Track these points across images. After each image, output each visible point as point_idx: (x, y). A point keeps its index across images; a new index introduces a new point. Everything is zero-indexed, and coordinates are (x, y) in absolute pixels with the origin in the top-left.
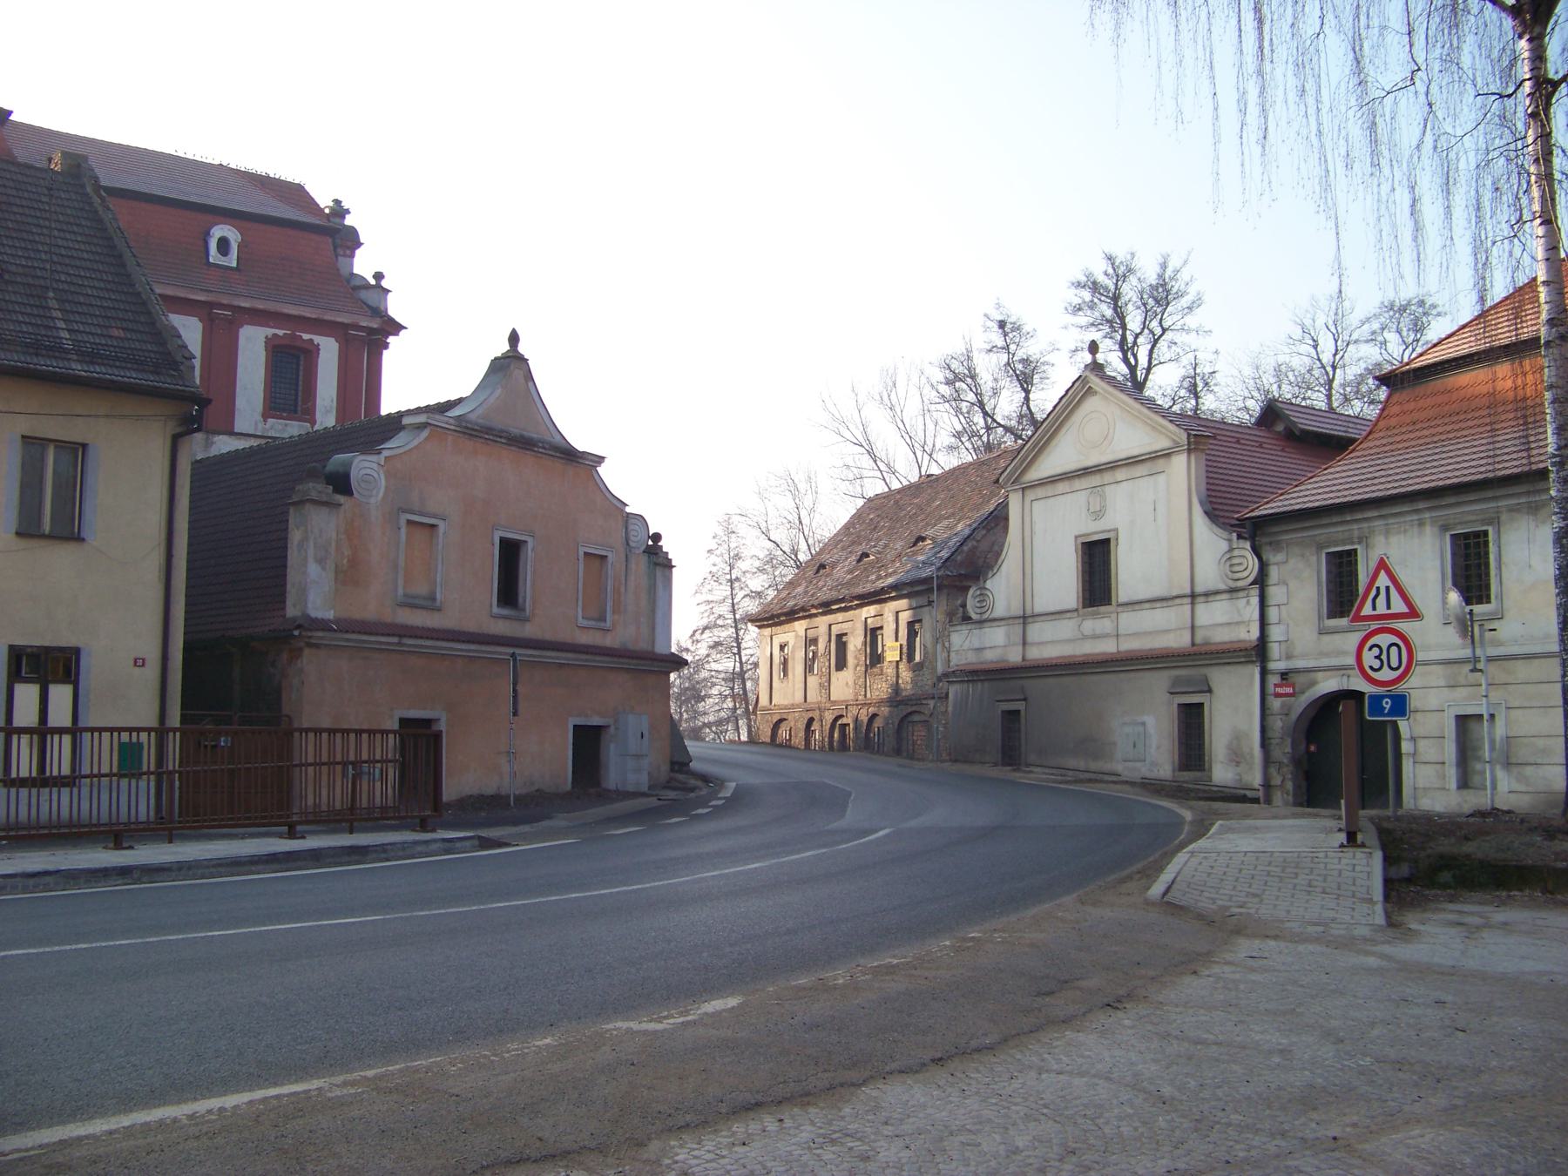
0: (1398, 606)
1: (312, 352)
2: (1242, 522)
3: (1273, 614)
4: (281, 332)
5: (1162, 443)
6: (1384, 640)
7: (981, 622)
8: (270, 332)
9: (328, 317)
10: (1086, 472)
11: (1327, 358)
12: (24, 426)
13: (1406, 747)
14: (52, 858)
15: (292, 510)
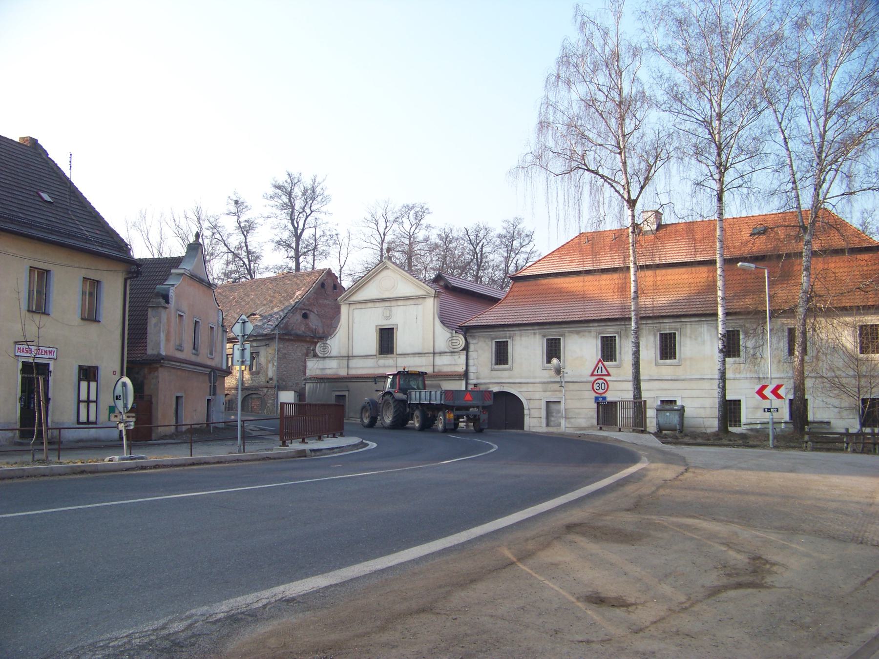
0: (604, 372)
2: (461, 327)
3: (471, 362)
5: (421, 293)
6: (600, 381)
7: (324, 358)
10: (383, 300)
11: (382, 231)
12: (84, 273)
13: (526, 412)
15: (149, 309)
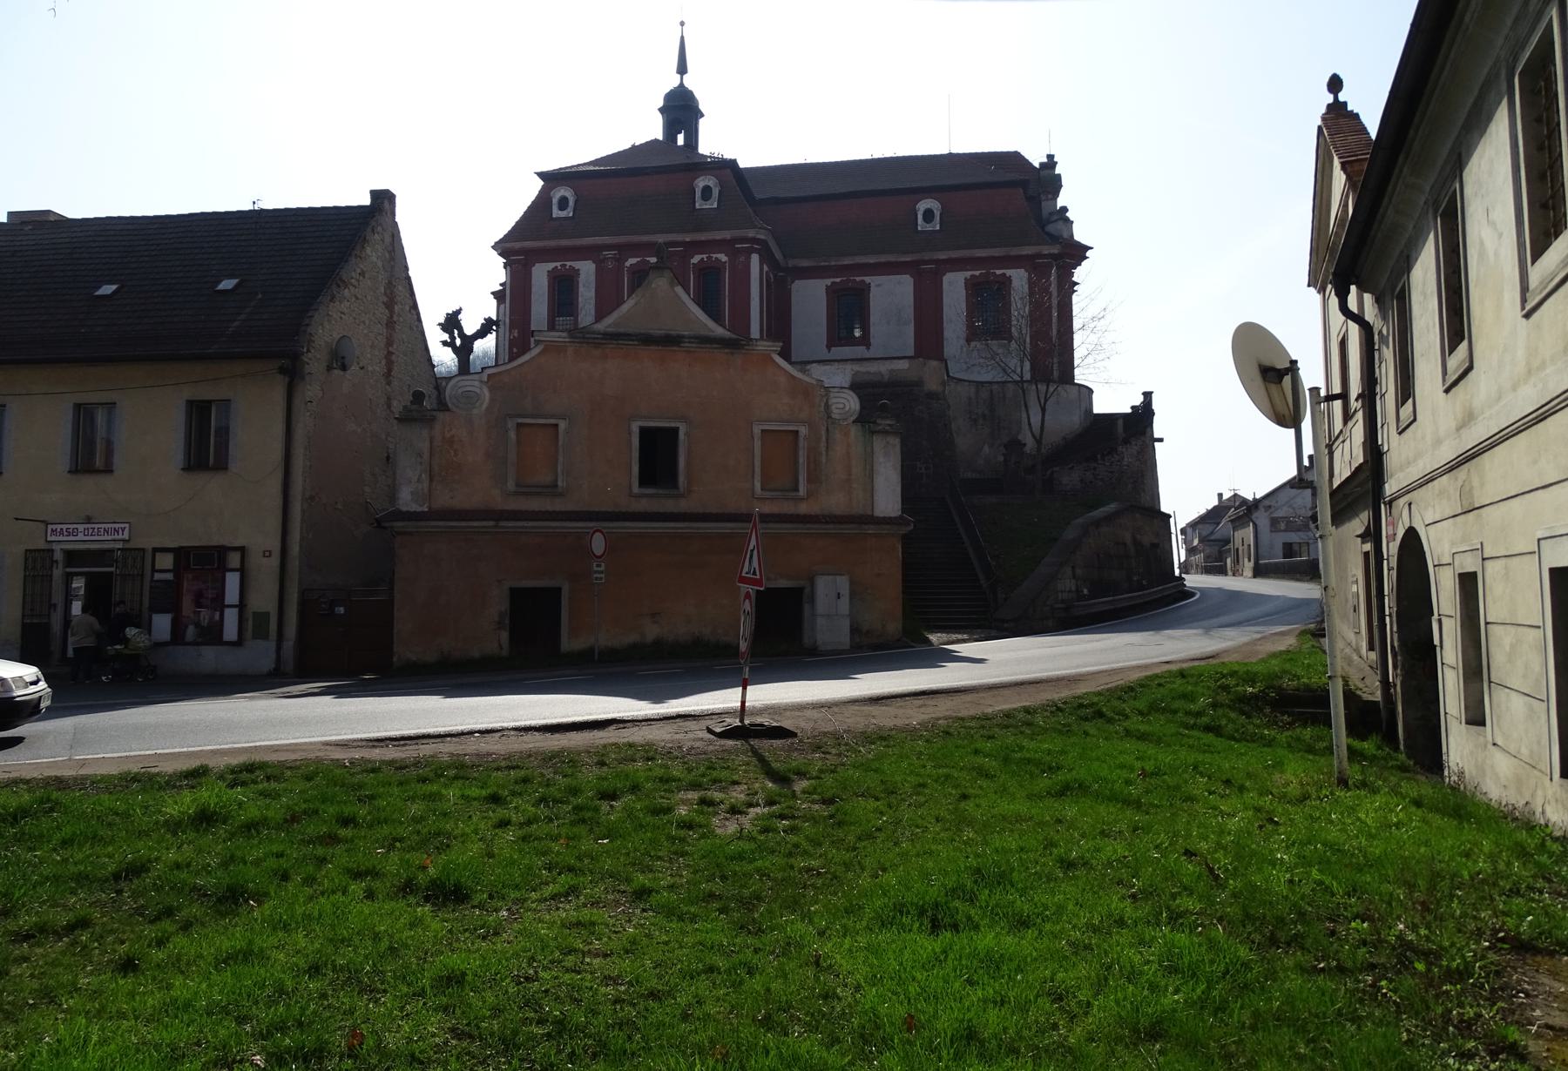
1: (1007, 281)
4: (977, 273)
8: (828, 282)
9: (1015, 251)
12: (188, 393)
14: (900, 712)
